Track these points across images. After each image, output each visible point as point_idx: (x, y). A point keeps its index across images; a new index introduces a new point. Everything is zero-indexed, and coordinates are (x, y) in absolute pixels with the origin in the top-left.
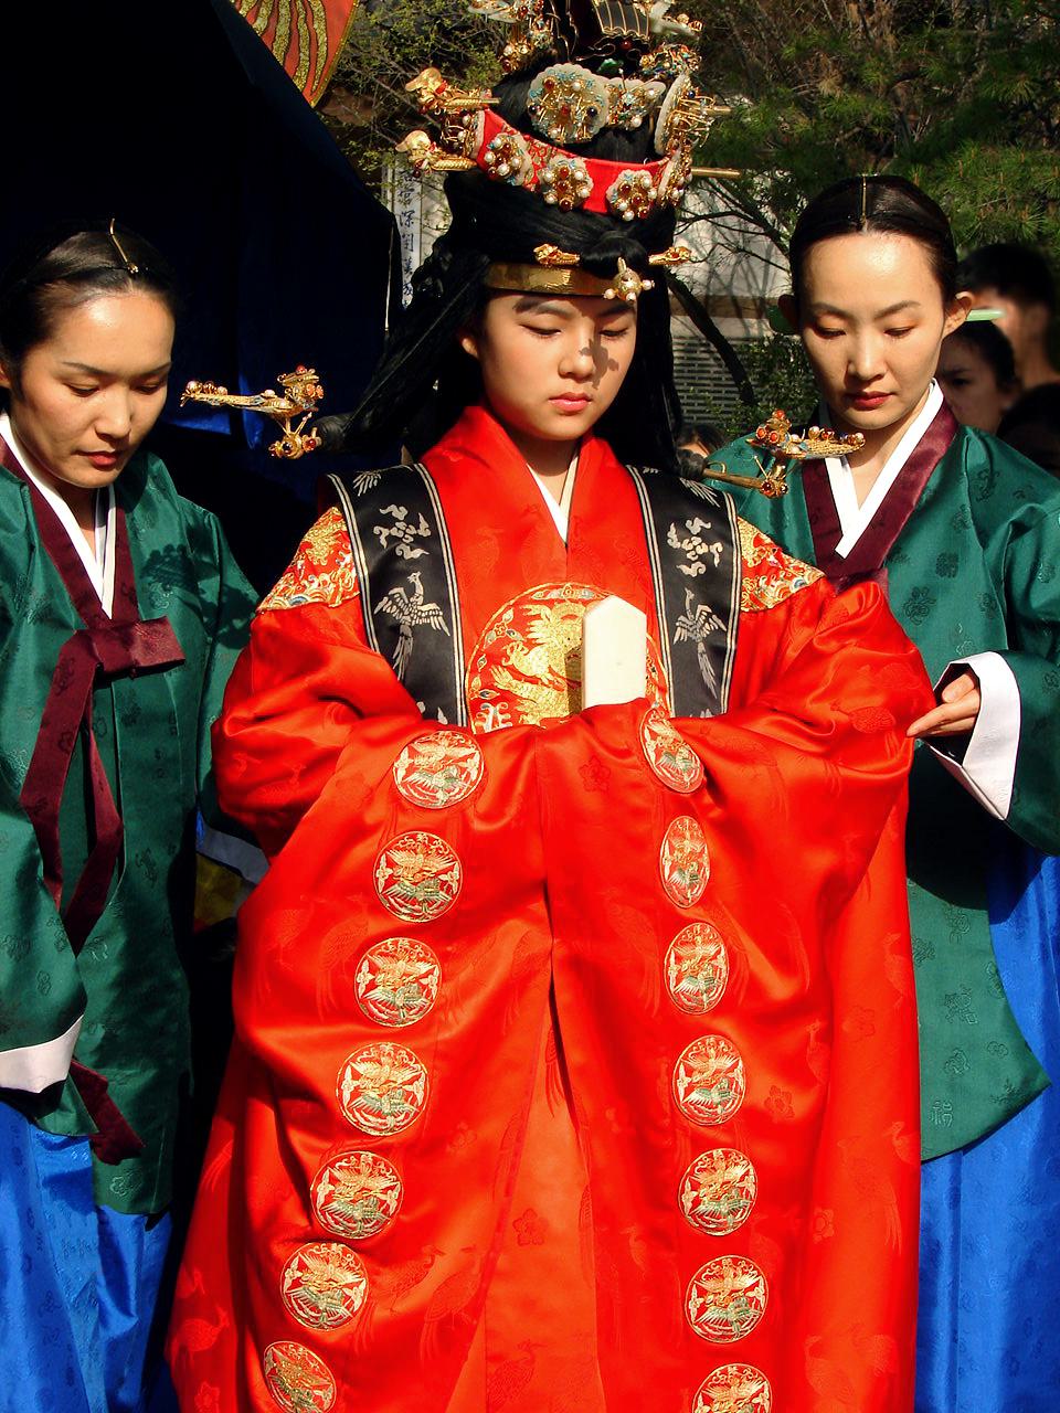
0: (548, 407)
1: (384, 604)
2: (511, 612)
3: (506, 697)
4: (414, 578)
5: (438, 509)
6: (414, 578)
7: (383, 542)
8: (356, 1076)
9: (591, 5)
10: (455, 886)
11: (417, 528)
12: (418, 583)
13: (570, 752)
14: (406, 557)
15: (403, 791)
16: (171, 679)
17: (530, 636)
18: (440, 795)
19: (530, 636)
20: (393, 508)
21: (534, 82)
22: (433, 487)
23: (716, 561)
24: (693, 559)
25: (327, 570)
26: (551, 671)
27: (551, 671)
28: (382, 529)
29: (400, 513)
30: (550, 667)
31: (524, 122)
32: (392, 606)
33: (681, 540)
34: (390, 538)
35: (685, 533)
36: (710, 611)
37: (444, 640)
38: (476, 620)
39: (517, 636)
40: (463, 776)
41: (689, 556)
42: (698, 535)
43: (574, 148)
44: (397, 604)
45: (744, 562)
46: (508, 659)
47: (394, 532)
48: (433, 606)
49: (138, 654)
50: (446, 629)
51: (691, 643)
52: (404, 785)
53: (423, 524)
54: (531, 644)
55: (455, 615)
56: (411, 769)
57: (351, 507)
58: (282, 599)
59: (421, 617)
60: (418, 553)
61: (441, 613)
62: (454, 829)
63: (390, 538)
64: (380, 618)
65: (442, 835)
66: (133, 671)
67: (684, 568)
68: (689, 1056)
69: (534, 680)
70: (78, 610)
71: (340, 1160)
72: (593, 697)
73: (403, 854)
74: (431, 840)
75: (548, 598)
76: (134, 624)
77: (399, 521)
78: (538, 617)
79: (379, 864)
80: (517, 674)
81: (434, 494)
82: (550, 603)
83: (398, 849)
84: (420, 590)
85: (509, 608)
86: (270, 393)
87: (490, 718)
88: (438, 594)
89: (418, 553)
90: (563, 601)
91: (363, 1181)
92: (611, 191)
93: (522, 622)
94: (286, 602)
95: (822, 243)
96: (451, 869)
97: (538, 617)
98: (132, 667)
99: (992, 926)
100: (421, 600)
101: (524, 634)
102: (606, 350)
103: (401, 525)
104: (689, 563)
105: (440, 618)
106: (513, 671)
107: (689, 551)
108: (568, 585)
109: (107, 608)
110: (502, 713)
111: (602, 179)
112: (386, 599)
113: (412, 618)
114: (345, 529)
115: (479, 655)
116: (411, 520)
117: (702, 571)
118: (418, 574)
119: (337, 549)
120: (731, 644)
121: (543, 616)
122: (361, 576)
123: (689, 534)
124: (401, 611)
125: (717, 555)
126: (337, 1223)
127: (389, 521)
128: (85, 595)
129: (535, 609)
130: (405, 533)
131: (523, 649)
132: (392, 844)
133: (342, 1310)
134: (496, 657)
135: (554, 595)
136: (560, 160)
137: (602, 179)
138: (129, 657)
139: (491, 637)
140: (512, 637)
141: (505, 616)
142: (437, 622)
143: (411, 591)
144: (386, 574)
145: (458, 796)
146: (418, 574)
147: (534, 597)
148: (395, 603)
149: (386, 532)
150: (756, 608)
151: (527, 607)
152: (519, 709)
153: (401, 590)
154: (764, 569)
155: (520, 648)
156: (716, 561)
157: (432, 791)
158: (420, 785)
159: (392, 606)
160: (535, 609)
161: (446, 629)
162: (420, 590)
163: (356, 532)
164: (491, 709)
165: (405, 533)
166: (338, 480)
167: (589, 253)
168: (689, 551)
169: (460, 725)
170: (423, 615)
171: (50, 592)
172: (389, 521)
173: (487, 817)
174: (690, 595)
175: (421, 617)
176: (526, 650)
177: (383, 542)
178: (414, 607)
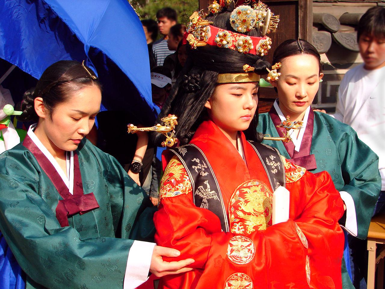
0: (240, 120)
3: (242, 220)
4: (206, 182)
5: (206, 159)
7: (197, 171)
9: (128, 1)
13: (276, 239)
14: (203, 175)
15: (231, 259)
16: (96, 213)
17: (246, 199)
18: (244, 259)
19: (246, 199)
20: (195, 159)
21: (232, 13)
22: (202, 151)
23: (279, 168)
24: (274, 168)
26: (254, 210)
27: (254, 210)
28: (195, 166)
30: (254, 209)
31: (229, 27)
32: (199, 192)
33: (270, 163)
34: (198, 169)
35: (270, 160)
37: (219, 203)
39: (241, 199)
40: (250, 252)
41: (273, 167)
42: (273, 161)
43: (246, 34)
44: (201, 192)
45: (285, 168)
46: (240, 207)
48: (213, 192)
49: (82, 208)
50: (218, 199)
52: (230, 257)
54: (247, 202)
55: (220, 194)
56: (232, 251)
57: (183, 160)
58: (170, 193)
59: (210, 196)
61: (216, 194)
62: (250, 270)
63: (198, 169)
64: (197, 197)
65: (246, 273)
66: (79, 212)
69: (249, 214)
70: (60, 193)
72: (276, 221)
73: (234, 281)
74: (243, 275)
75: (248, 186)
76: (81, 196)
77: (199, 163)
79: (225, 285)
80: (245, 213)
81: (203, 154)
82: (249, 187)
83: (232, 280)
84: (208, 186)
85: (237, 191)
86: (159, 125)
87: (237, 228)
89: (206, 174)
90: (252, 186)
92: (258, 46)
93: (242, 195)
94: (172, 194)
95: (285, 58)
96: (250, 285)
97: (246, 192)
98: (80, 211)
99: (122, 238)
100: (209, 190)
101: (244, 198)
103: (199, 164)
105: (216, 196)
106: (242, 211)
107: (272, 166)
108: (252, 180)
109: (71, 191)
110: (240, 226)
111: (255, 43)
112: (197, 190)
113: (207, 197)
114: (183, 167)
115: (231, 207)
117: (276, 172)
118: (207, 181)
119: (183, 174)
121: (248, 192)
122: (192, 182)
124: (203, 194)
125: (279, 166)
128: (63, 188)
129: (245, 190)
130: (202, 167)
131: (244, 204)
132: (230, 278)
134: (237, 207)
135: (250, 184)
136: (242, 37)
137: (255, 43)
138: (79, 208)
139: (233, 201)
140: (240, 200)
141: (237, 193)
142: (215, 197)
143: (205, 187)
144: (199, 181)
145: (250, 259)
146: (207, 181)
147: (245, 186)
148: (200, 191)
151: (242, 189)
152: (246, 224)
153: (202, 187)
154: (291, 170)
155: (243, 204)
157: (240, 258)
158: (236, 256)
159: (199, 192)
160: (245, 190)
161: (218, 199)
162: (208, 186)
163: (187, 168)
164: (237, 224)
165: (202, 167)
166: (174, 151)
167: (257, 67)
168: (272, 166)
169: (227, 231)
170: (211, 195)
171: (48, 187)
172: (196, 164)
173: (259, 264)
175: (210, 196)
176: (246, 204)
177: (197, 171)
178: (207, 193)
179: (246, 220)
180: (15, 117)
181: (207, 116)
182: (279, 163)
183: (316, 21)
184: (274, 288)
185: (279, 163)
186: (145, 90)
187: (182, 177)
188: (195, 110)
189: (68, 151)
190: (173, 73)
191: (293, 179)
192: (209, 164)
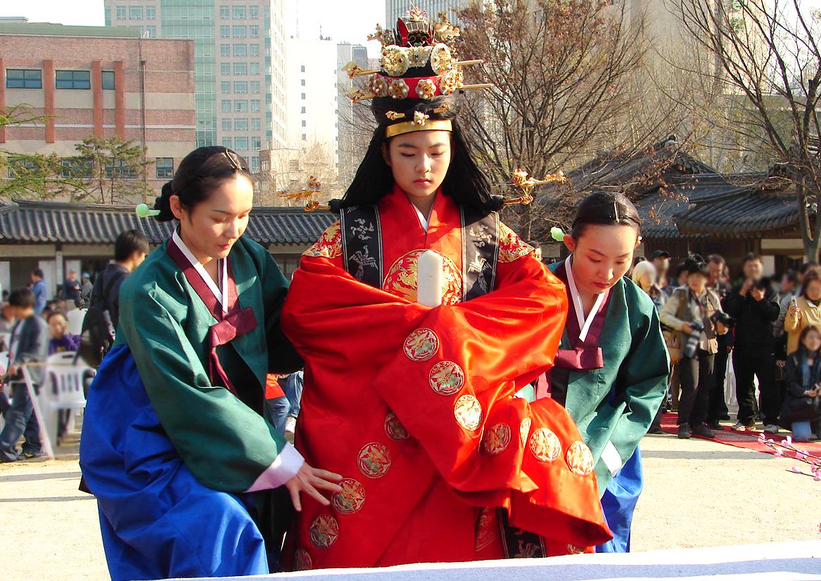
2: (402, 261)
5: (378, 222)
6: (365, 247)
8: (370, 450)
10: (540, 457)
11: (368, 228)
12: (366, 249)
25: (331, 244)
29: (362, 222)
36: (624, 405)
38: (388, 262)
39: (404, 269)
47: (359, 229)
48: (372, 258)
53: (371, 226)
54: (409, 273)
60: (367, 238)
68: (84, 342)
71: (347, 480)
78: (412, 263)
80: (403, 285)
84: (367, 252)
88: (374, 253)
89: (367, 238)
91: (351, 491)
97: (412, 263)
100: (367, 256)
102: (548, 392)
103: (362, 227)
106: (401, 283)
116: (367, 225)
120: (494, 273)
124: (360, 260)
126: (336, 503)
127: (358, 225)
133: (326, 544)
134: (395, 277)
139: (394, 270)
142: (373, 264)
143: (364, 252)
149: (355, 229)
150: (506, 261)
153: (360, 252)
162: (367, 252)
172: (358, 225)
179: (316, 141)
180: (127, 537)
181: (679, 348)
183: (54, 262)
184: (519, 541)
186: (738, 44)
187: (334, 240)
188: (595, 86)
189: (155, 216)
190: (93, 307)
191: (508, 259)
192: (379, 229)
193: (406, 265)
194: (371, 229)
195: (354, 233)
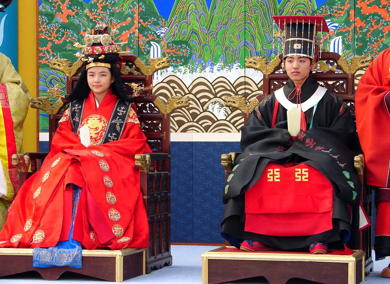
1: (74, 119)
5: (84, 105)
23: (124, 113)
39: (86, 122)
47: (75, 108)
51: (115, 124)
54: (87, 123)
67: (119, 114)
104: (120, 113)
116: (78, 106)
123: (121, 109)
149: (74, 108)
156: (124, 113)
160: (89, 118)
174: (118, 117)
182: (125, 111)
185: (125, 111)
192: (83, 107)
193: (87, 121)
194: (80, 107)
195: (73, 110)
